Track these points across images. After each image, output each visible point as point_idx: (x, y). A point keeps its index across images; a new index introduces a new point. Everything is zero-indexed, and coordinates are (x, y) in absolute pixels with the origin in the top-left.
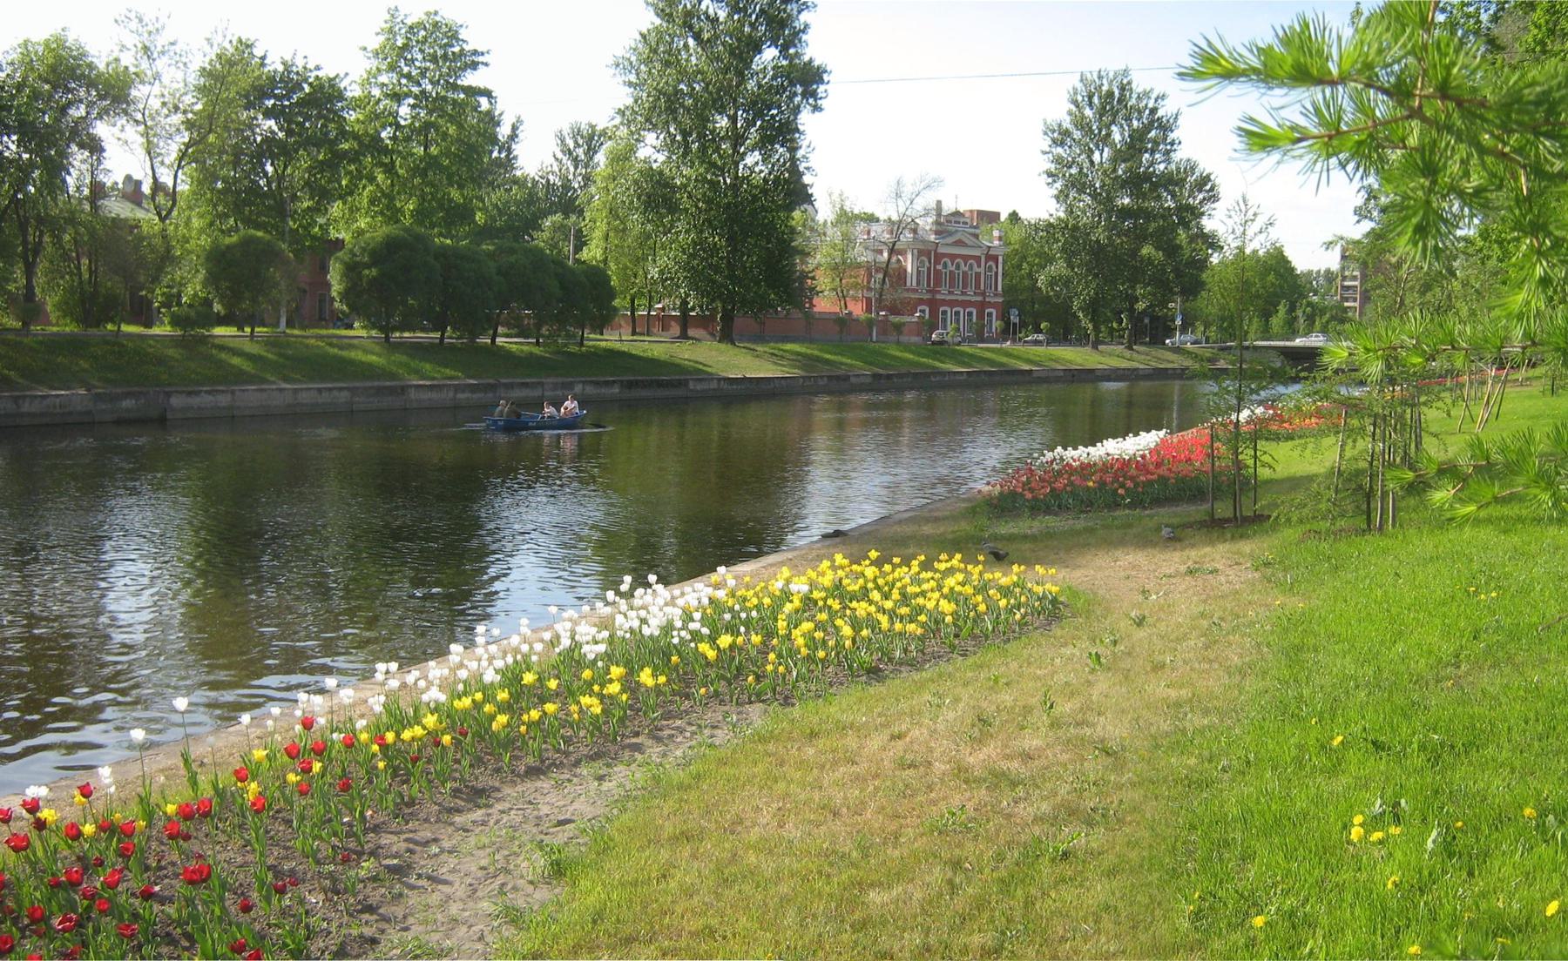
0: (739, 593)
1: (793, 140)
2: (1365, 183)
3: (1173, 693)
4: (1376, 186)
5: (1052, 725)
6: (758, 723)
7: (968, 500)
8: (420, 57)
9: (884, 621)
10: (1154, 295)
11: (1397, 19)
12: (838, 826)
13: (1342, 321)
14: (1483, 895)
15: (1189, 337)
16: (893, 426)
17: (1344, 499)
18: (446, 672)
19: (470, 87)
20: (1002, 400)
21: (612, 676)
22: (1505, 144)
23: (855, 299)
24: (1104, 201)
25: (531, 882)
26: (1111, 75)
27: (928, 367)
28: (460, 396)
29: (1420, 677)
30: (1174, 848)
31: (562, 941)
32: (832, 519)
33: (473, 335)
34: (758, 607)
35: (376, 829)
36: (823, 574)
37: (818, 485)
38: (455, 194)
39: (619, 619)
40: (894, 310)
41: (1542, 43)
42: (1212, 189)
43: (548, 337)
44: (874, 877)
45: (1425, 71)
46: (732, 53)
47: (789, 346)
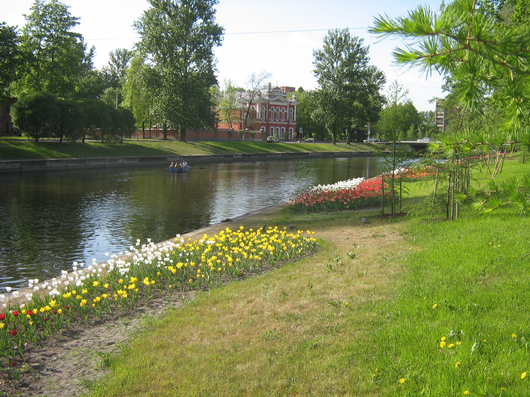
0: (186, 245)
1: (210, 58)
2: (446, 75)
3: (366, 286)
4: (451, 77)
5: (312, 294)
6: (193, 298)
7: (282, 206)
8: (50, 19)
9: (245, 255)
10: (359, 122)
11: (459, 8)
12: (224, 339)
13: (437, 133)
14: (495, 370)
15: (373, 139)
16: (250, 176)
17: (437, 206)
18: (60, 282)
19: (72, 33)
20: (296, 165)
21: (132, 281)
22: (504, 59)
23: (235, 123)
24: (338, 83)
25: (96, 370)
26: (341, 31)
27: (265, 151)
28: (69, 165)
29: (469, 280)
30: (367, 350)
31: (108, 393)
32: (225, 214)
33: (75, 138)
34: (194, 251)
35: (29, 351)
36: (221, 236)
37: (220, 200)
38: (66, 78)
39: (135, 257)
40: (251, 128)
41: (519, 18)
42: (383, 78)
43: (107, 140)
44: (239, 359)
45: (471, 29)
46: (183, 21)
47: (209, 143)
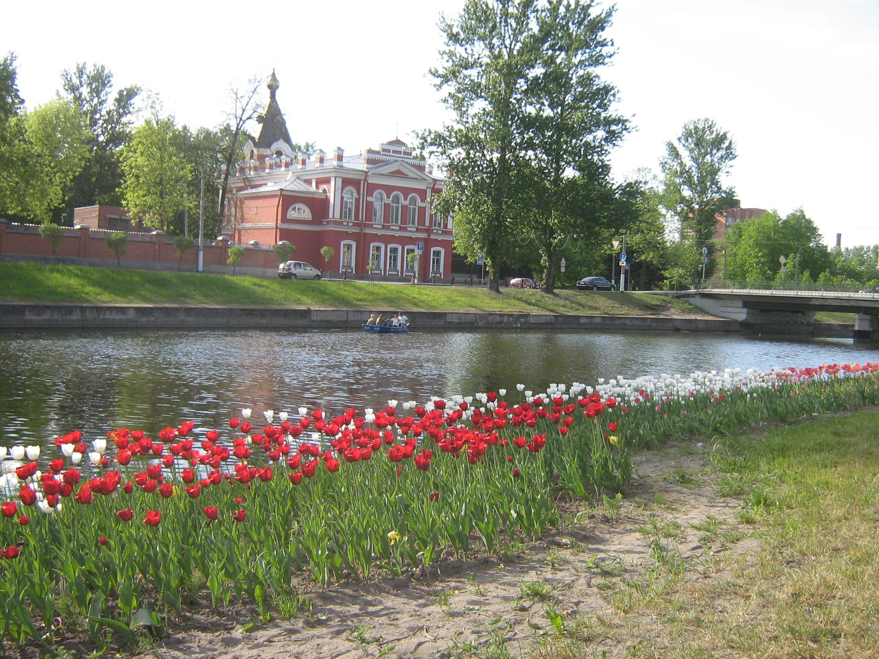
42: (729, 147)
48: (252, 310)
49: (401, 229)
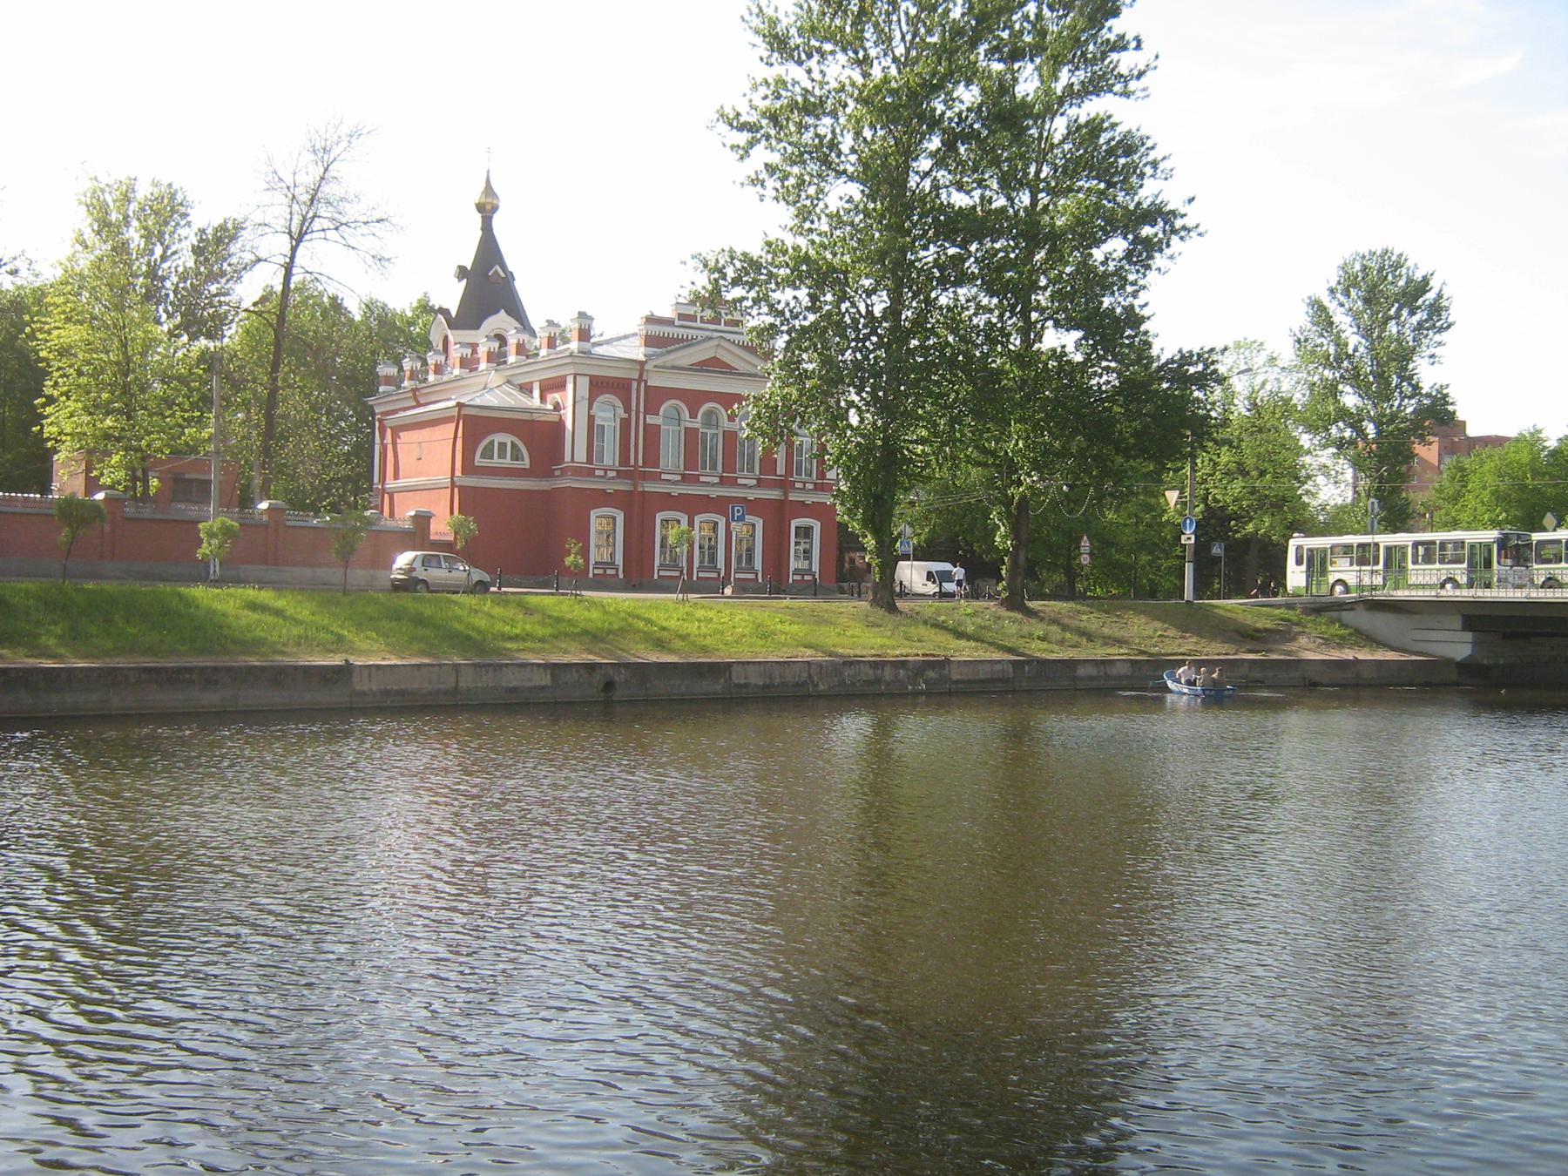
48: (179, 671)
49: (723, 481)
